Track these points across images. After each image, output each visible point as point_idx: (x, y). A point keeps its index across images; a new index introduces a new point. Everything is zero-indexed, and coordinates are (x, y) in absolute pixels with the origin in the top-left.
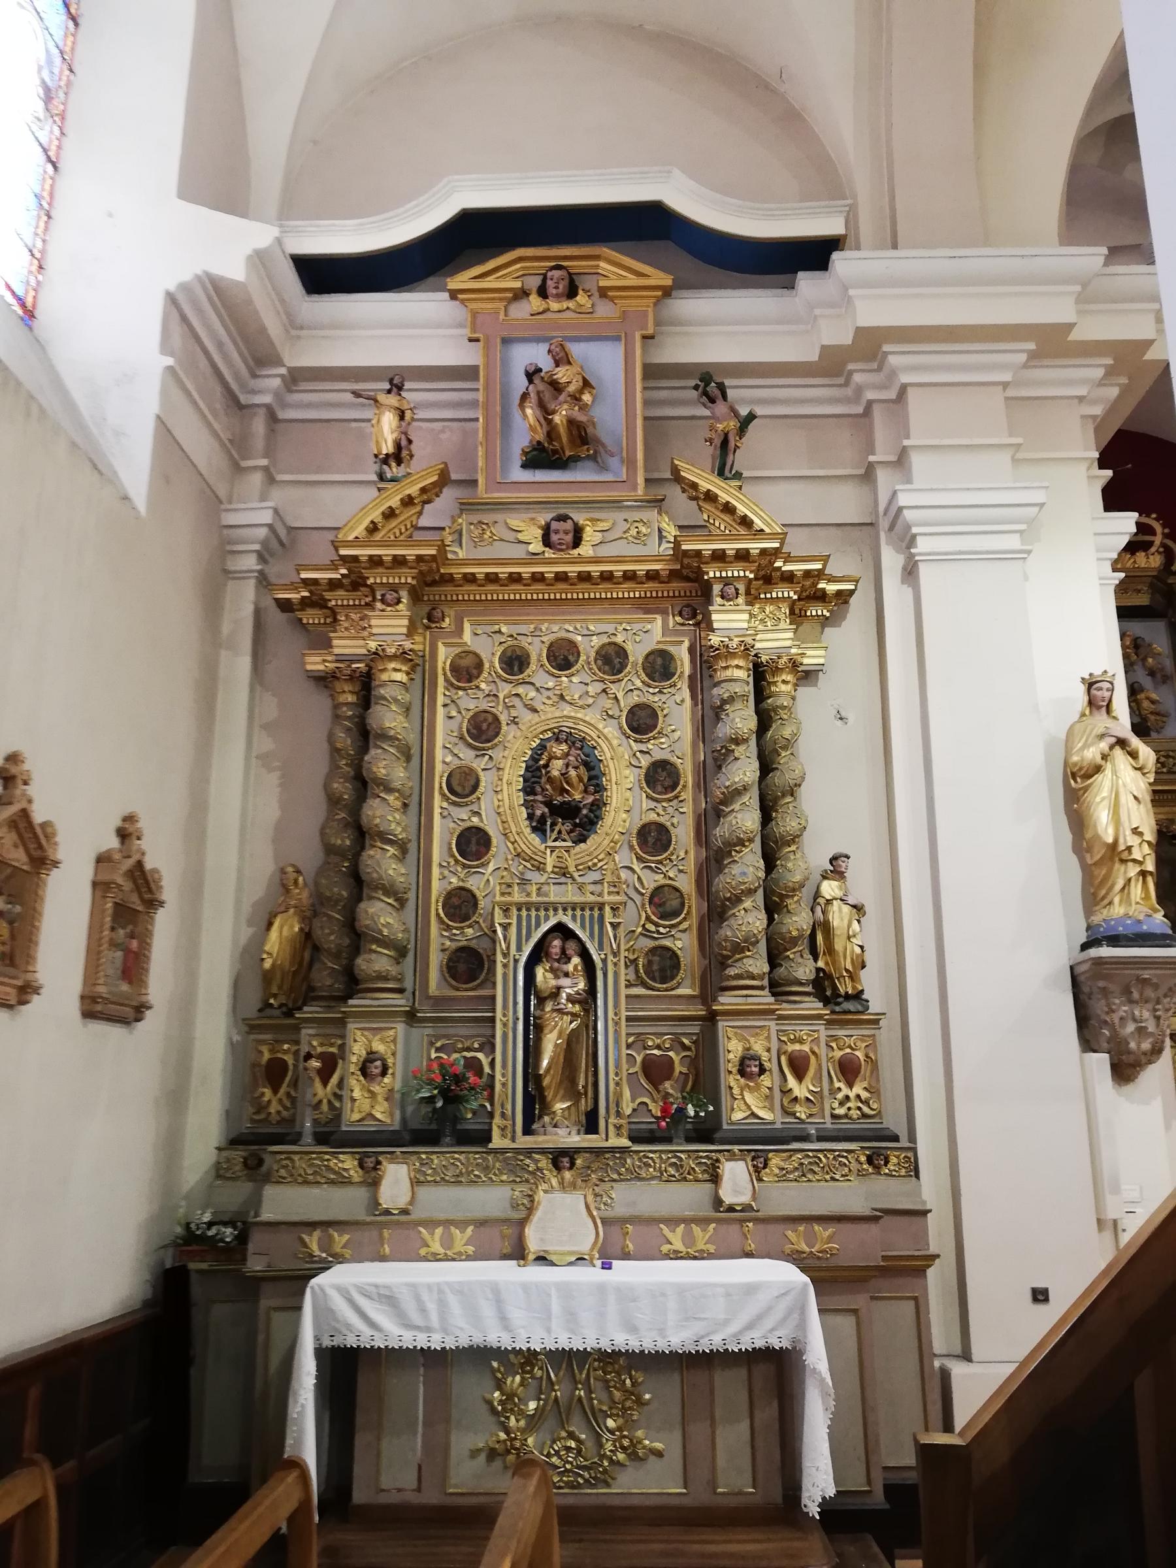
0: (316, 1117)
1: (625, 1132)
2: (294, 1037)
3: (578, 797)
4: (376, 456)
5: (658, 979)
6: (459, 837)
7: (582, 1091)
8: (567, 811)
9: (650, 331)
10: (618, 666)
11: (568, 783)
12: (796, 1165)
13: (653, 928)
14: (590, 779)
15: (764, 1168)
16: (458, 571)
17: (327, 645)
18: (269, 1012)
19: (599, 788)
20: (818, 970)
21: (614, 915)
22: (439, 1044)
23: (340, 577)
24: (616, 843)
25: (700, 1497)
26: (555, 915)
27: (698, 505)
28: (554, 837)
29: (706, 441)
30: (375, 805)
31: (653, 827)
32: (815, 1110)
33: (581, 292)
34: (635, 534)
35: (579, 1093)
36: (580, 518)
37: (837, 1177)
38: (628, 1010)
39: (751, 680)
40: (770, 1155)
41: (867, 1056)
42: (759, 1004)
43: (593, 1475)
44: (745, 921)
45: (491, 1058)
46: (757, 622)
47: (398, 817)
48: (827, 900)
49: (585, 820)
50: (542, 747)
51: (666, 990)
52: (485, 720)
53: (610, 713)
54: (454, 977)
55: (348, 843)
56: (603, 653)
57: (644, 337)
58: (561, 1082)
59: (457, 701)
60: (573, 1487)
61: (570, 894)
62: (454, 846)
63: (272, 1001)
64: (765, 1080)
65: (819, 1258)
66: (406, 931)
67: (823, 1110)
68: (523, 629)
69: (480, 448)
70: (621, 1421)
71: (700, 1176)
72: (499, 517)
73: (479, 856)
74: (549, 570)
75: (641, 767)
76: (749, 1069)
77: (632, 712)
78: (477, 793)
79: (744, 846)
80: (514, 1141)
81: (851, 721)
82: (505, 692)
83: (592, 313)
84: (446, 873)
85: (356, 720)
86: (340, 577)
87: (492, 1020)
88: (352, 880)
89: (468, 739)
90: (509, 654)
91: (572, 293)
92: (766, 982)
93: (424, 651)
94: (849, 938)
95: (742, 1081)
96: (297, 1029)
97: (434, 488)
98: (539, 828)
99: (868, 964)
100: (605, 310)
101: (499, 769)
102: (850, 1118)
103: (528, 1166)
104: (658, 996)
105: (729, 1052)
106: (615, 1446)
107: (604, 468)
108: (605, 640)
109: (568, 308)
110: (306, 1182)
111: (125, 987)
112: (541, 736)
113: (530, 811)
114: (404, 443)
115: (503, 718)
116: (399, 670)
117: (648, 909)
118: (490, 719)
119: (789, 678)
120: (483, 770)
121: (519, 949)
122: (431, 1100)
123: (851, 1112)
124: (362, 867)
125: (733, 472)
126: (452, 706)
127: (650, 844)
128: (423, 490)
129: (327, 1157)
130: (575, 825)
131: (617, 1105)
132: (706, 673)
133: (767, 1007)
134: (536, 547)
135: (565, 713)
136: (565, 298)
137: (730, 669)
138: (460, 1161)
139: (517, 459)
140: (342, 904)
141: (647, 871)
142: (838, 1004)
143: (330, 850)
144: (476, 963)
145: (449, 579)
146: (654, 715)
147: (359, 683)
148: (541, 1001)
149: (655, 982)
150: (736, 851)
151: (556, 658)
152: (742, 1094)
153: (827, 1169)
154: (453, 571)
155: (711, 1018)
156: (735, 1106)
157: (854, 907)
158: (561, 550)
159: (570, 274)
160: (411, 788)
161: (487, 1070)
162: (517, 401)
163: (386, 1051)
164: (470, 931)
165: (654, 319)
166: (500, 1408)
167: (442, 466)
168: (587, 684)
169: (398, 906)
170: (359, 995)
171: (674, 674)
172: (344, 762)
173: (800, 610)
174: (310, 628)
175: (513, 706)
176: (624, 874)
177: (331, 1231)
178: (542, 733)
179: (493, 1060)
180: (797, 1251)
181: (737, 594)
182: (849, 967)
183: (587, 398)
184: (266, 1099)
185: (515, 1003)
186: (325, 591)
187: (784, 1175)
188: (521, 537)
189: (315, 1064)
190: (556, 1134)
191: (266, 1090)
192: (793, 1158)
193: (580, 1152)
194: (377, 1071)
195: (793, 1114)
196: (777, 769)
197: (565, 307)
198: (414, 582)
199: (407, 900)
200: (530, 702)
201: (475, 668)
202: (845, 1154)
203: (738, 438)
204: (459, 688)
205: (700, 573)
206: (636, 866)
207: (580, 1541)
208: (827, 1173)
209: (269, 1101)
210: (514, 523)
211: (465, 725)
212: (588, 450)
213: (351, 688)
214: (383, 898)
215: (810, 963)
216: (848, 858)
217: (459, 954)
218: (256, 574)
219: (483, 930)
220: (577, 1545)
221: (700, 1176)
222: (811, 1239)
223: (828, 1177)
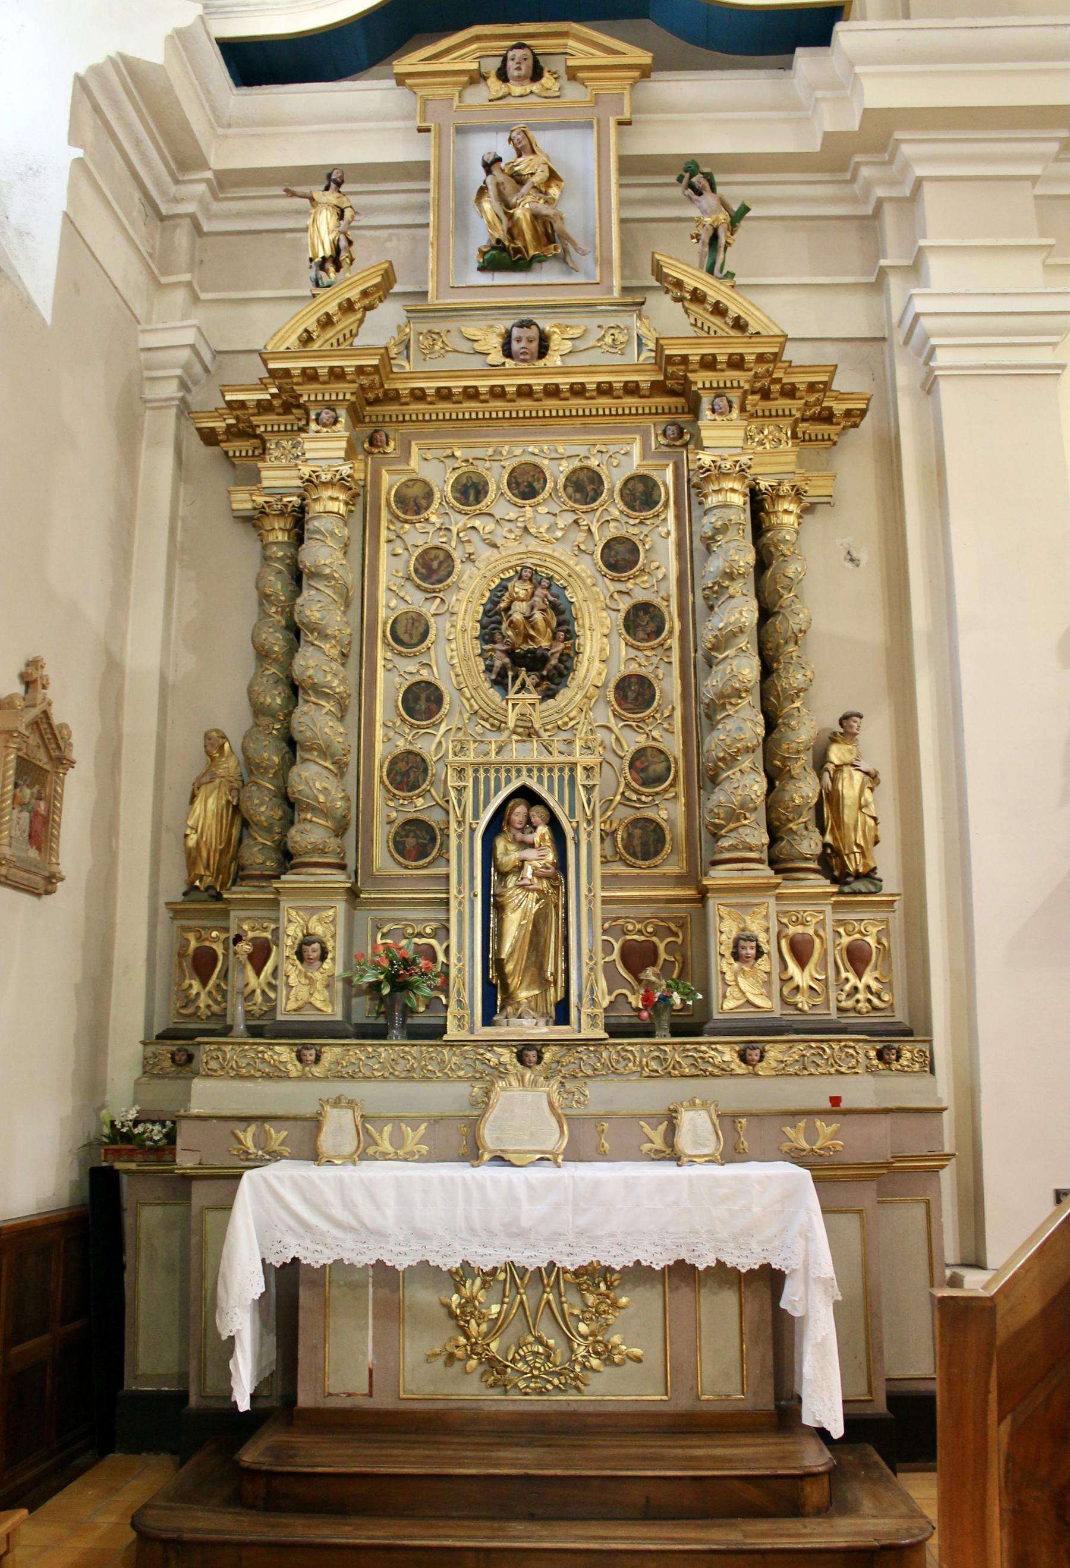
0: (250, 1008)
1: (601, 1021)
2: (222, 924)
3: (545, 644)
4: (311, 260)
5: (639, 855)
6: (406, 693)
7: (551, 979)
8: (534, 661)
9: (627, 115)
10: (591, 494)
11: (533, 628)
12: (797, 1057)
13: (634, 797)
14: (559, 624)
15: (760, 1060)
16: (403, 387)
17: (254, 478)
18: (195, 895)
19: (570, 635)
20: (825, 845)
21: (588, 777)
22: (385, 930)
23: (269, 397)
24: (590, 699)
25: (684, 1403)
26: (518, 777)
27: (684, 306)
28: (516, 688)
29: (692, 238)
30: (308, 654)
31: (633, 680)
32: (819, 1000)
33: (546, 74)
34: (610, 341)
35: (547, 981)
36: (547, 325)
37: (843, 1069)
38: (603, 889)
39: (748, 507)
40: (767, 1047)
41: (879, 942)
42: (757, 878)
43: (563, 1381)
44: (741, 784)
45: (445, 945)
46: (755, 444)
47: (334, 667)
48: (837, 766)
49: (554, 672)
50: (503, 587)
51: (649, 868)
52: (436, 557)
53: (583, 547)
54: (401, 853)
55: (279, 701)
56: (574, 479)
57: (620, 123)
58: (526, 967)
59: (403, 536)
60: (541, 1393)
61: (533, 752)
62: (400, 704)
63: (197, 883)
64: (763, 964)
65: (821, 1155)
66: (346, 799)
67: (828, 1000)
68: (479, 452)
69: (430, 250)
70: (594, 1326)
71: (687, 1070)
72: (452, 325)
73: (430, 714)
74: (510, 383)
75: (619, 611)
76: (744, 952)
77: (607, 546)
78: (427, 642)
79: (740, 697)
80: (472, 1033)
81: (863, 563)
82: (460, 525)
83: (558, 97)
84: (391, 734)
85: (288, 561)
86: (269, 397)
87: (446, 902)
88: (284, 744)
89: (416, 579)
90: (464, 481)
91: (537, 74)
92: (765, 856)
93: (365, 480)
94: (860, 808)
95: (736, 965)
96: (226, 914)
97: (378, 291)
98: (500, 682)
99: (881, 838)
100: (574, 93)
101: (453, 614)
102: (859, 1012)
103: (489, 1060)
104: (639, 876)
105: (721, 932)
106: (588, 1352)
107: (572, 270)
108: (576, 463)
109: (531, 92)
110: (240, 1077)
111: (33, 853)
112: (502, 576)
113: (488, 662)
114: (343, 243)
115: (457, 555)
116: (336, 499)
117: (628, 774)
118: (442, 556)
119: (792, 507)
120: (434, 615)
121: (476, 816)
122: (375, 986)
123: (860, 1005)
124: (295, 724)
125: (725, 272)
126: (398, 540)
127: (629, 700)
128: (365, 294)
129: (261, 1048)
130: (542, 678)
131: (592, 992)
132: (695, 500)
133: (765, 881)
134: (497, 357)
135: (530, 548)
136: (528, 80)
137: (723, 493)
138: (411, 1055)
139: (475, 260)
140: (273, 771)
141: (627, 731)
142: (847, 884)
143: (259, 710)
144: (428, 837)
145: (393, 397)
146: (635, 550)
147: (290, 519)
148: (503, 875)
149: (636, 857)
150: (731, 704)
151: (518, 484)
152: (736, 981)
153: (831, 1061)
154: (398, 385)
155: (703, 896)
156: (728, 994)
157: (867, 773)
158: (524, 361)
159: (534, 55)
160: (351, 635)
161: (441, 958)
162: (474, 196)
163: (324, 932)
164: (420, 802)
165: (631, 106)
166: (458, 1311)
167: (386, 265)
168: (555, 515)
169: (336, 771)
170: (294, 871)
171: (657, 503)
172: (273, 610)
173: (804, 433)
174: (237, 462)
175: (469, 541)
176: (600, 734)
177: (267, 1126)
178: (502, 571)
179: (448, 947)
180: (797, 1149)
181: (731, 407)
182: (862, 842)
183: (554, 191)
184: (194, 991)
185: (472, 878)
186: (253, 415)
187: (784, 1069)
188: (477, 347)
189: (245, 947)
190: (521, 1025)
191: (193, 982)
192: (794, 1050)
193: (548, 1045)
194: (317, 954)
195: (795, 1006)
196: (778, 612)
197: (528, 91)
198: (353, 399)
199: (346, 764)
200: (488, 536)
201: (424, 498)
202: (852, 1044)
203: (729, 234)
204: (406, 521)
205: (687, 383)
206: (612, 722)
207: (549, 1446)
208: (832, 1066)
209: (198, 994)
210: (470, 330)
211: (412, 563)
212: (555, 249)
213: (282, 526)
214: (318, 760)
215: (816, 835)
216: (860, 717)
217: (407, 827)
218: (177, 402)
219: (435, 800)
220: (546, 1449)
221: (687, 1070)
222: (811, 1134)
223: (833, 1070)
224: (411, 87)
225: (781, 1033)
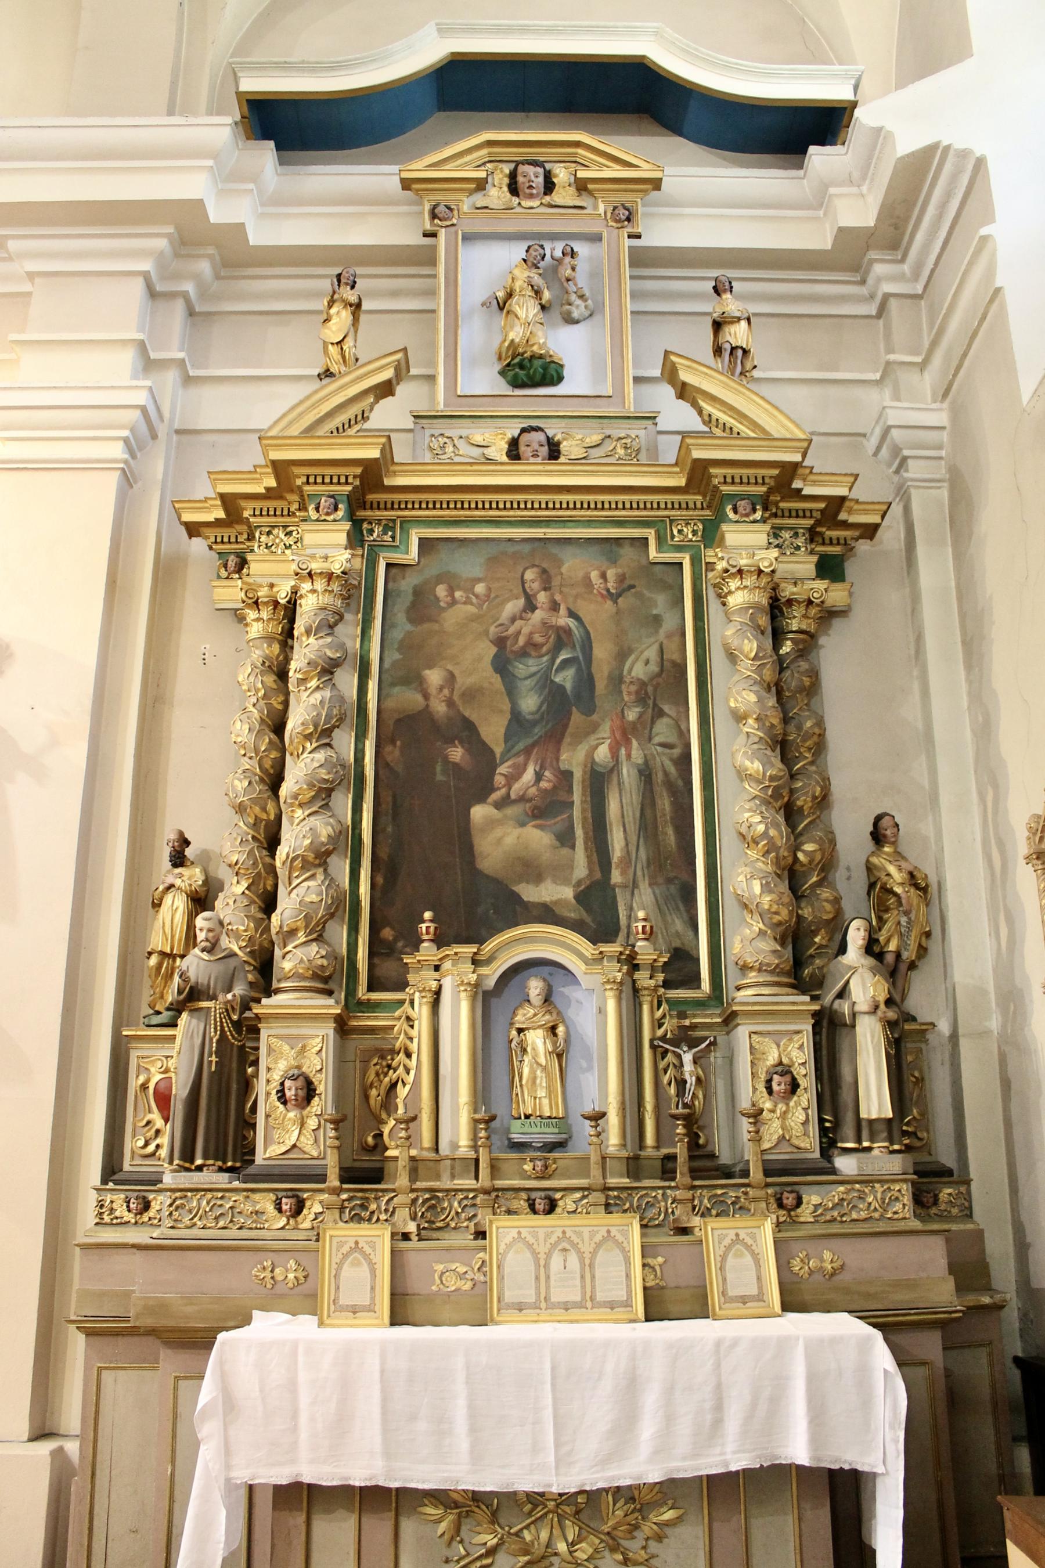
224: (417, 190)
225: (271, 265)
